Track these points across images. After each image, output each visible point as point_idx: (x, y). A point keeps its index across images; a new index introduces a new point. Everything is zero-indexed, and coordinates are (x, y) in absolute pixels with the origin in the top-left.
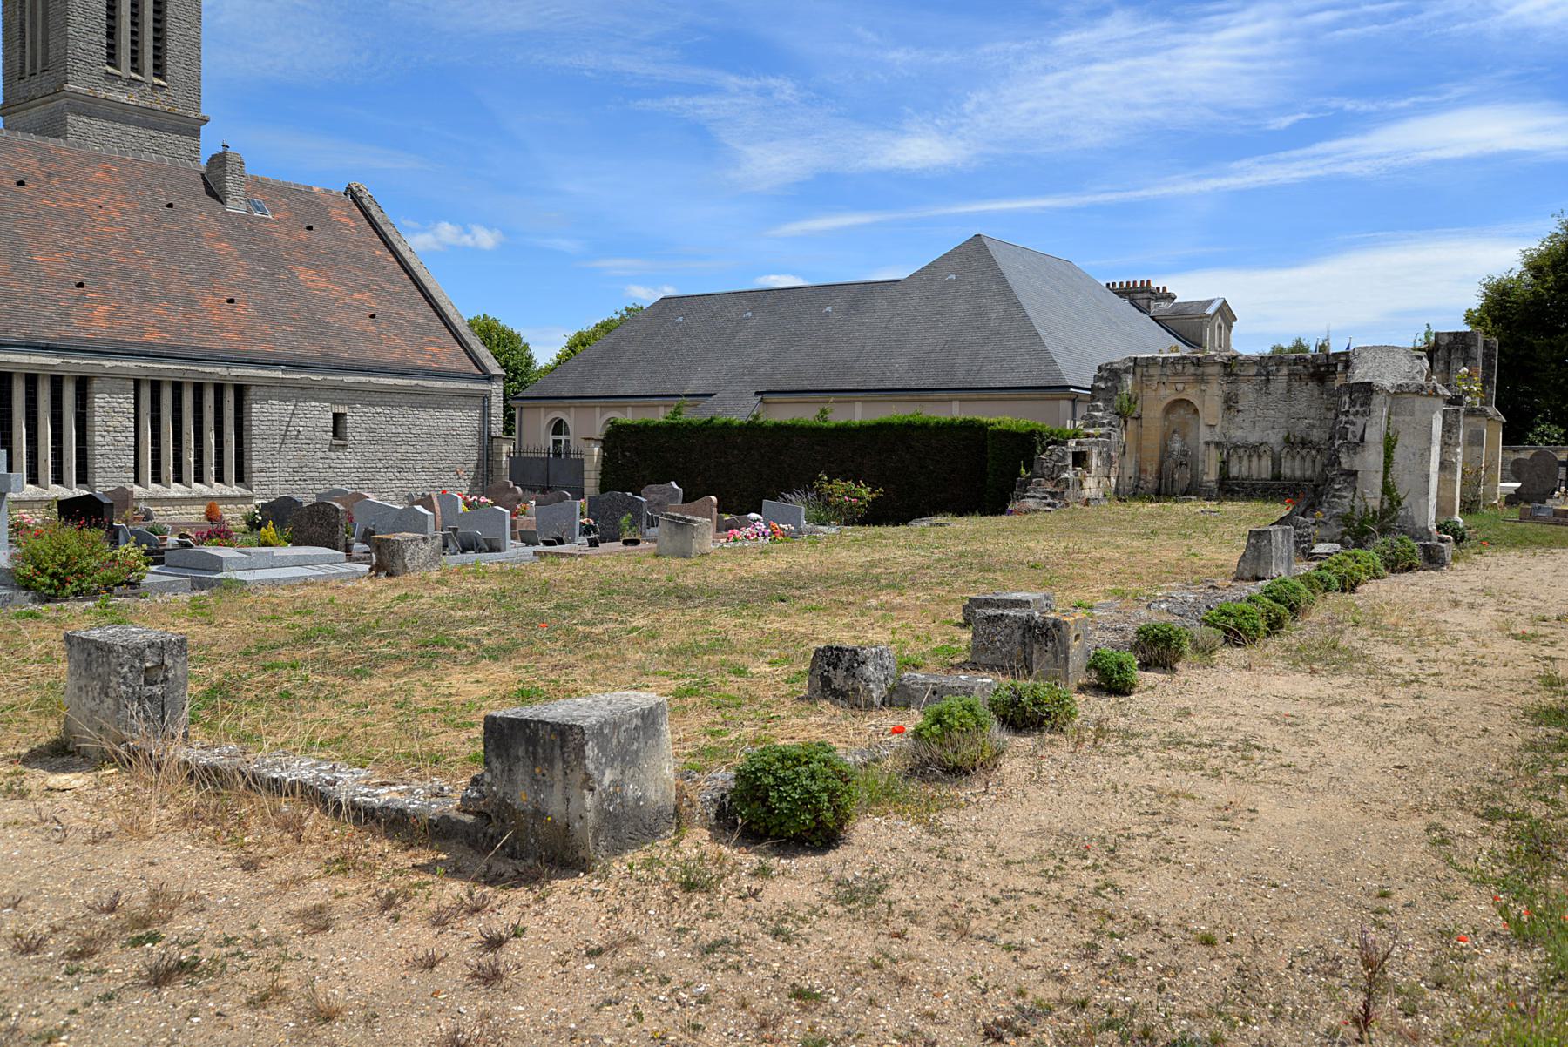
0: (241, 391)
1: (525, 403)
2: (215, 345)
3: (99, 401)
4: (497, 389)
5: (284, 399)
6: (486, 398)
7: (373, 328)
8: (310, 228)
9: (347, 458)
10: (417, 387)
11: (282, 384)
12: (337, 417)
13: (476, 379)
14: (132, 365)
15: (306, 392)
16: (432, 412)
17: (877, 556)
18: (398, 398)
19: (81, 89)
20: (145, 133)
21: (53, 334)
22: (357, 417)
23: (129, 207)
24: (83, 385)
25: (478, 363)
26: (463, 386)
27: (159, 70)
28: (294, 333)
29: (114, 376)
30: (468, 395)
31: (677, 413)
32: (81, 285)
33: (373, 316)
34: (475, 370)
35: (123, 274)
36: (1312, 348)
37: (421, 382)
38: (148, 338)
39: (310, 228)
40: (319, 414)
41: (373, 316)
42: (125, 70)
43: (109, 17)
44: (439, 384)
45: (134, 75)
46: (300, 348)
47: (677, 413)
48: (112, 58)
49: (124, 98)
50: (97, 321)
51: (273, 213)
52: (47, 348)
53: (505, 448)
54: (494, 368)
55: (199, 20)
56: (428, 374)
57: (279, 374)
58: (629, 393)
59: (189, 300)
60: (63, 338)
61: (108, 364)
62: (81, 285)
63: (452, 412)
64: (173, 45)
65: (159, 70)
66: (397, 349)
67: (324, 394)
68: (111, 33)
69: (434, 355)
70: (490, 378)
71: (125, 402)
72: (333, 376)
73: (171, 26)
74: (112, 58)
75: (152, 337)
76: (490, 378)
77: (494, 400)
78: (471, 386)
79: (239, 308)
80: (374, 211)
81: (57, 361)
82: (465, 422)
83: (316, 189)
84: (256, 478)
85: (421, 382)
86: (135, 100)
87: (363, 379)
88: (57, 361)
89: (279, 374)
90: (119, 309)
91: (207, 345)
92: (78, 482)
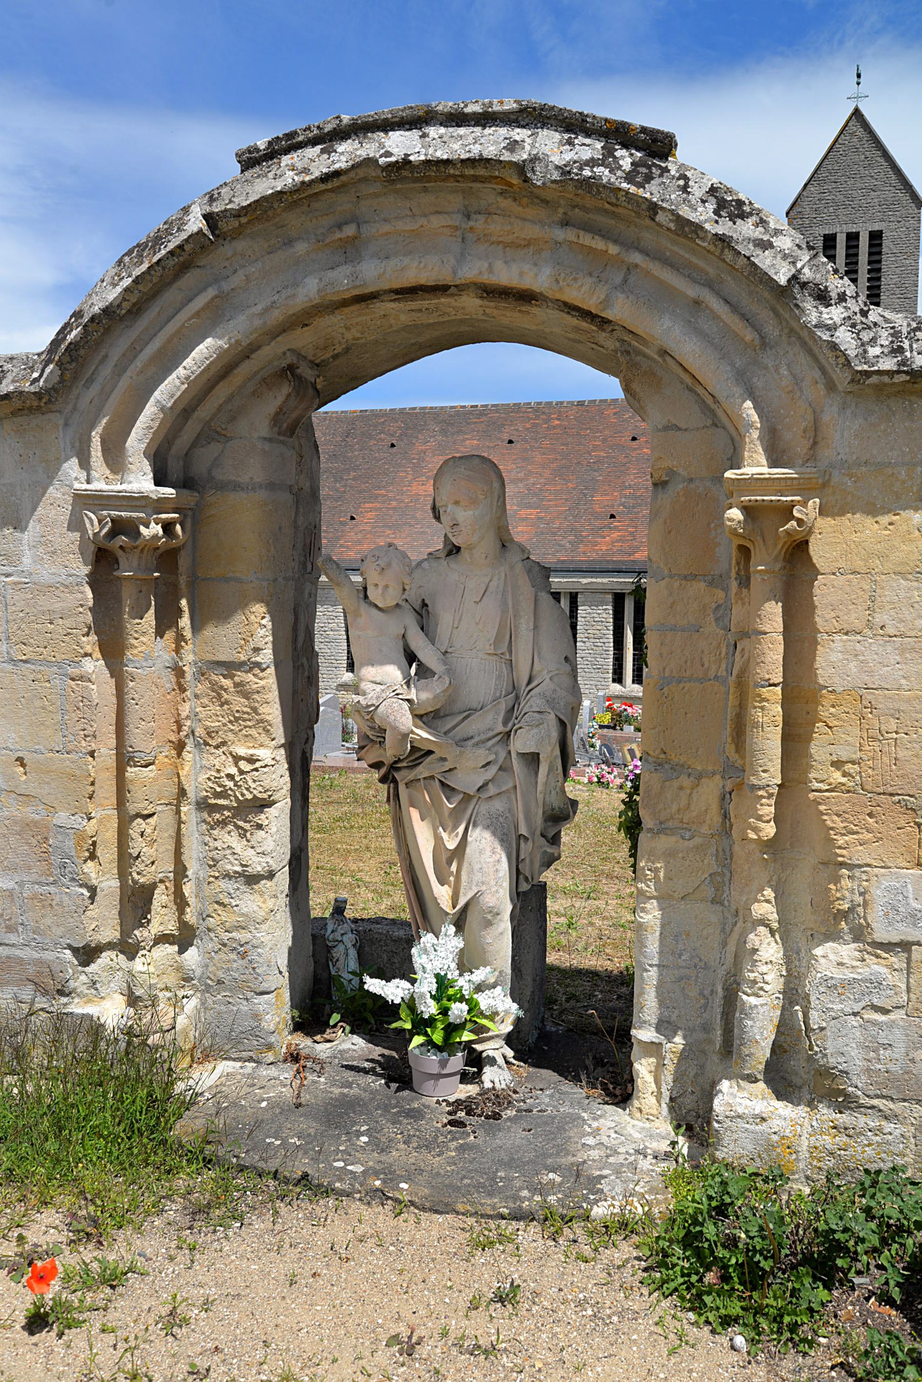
14: (605, 580)
61: (584, 581)
62: (612, 516)
71: (606, 614)
90: (631, 533)
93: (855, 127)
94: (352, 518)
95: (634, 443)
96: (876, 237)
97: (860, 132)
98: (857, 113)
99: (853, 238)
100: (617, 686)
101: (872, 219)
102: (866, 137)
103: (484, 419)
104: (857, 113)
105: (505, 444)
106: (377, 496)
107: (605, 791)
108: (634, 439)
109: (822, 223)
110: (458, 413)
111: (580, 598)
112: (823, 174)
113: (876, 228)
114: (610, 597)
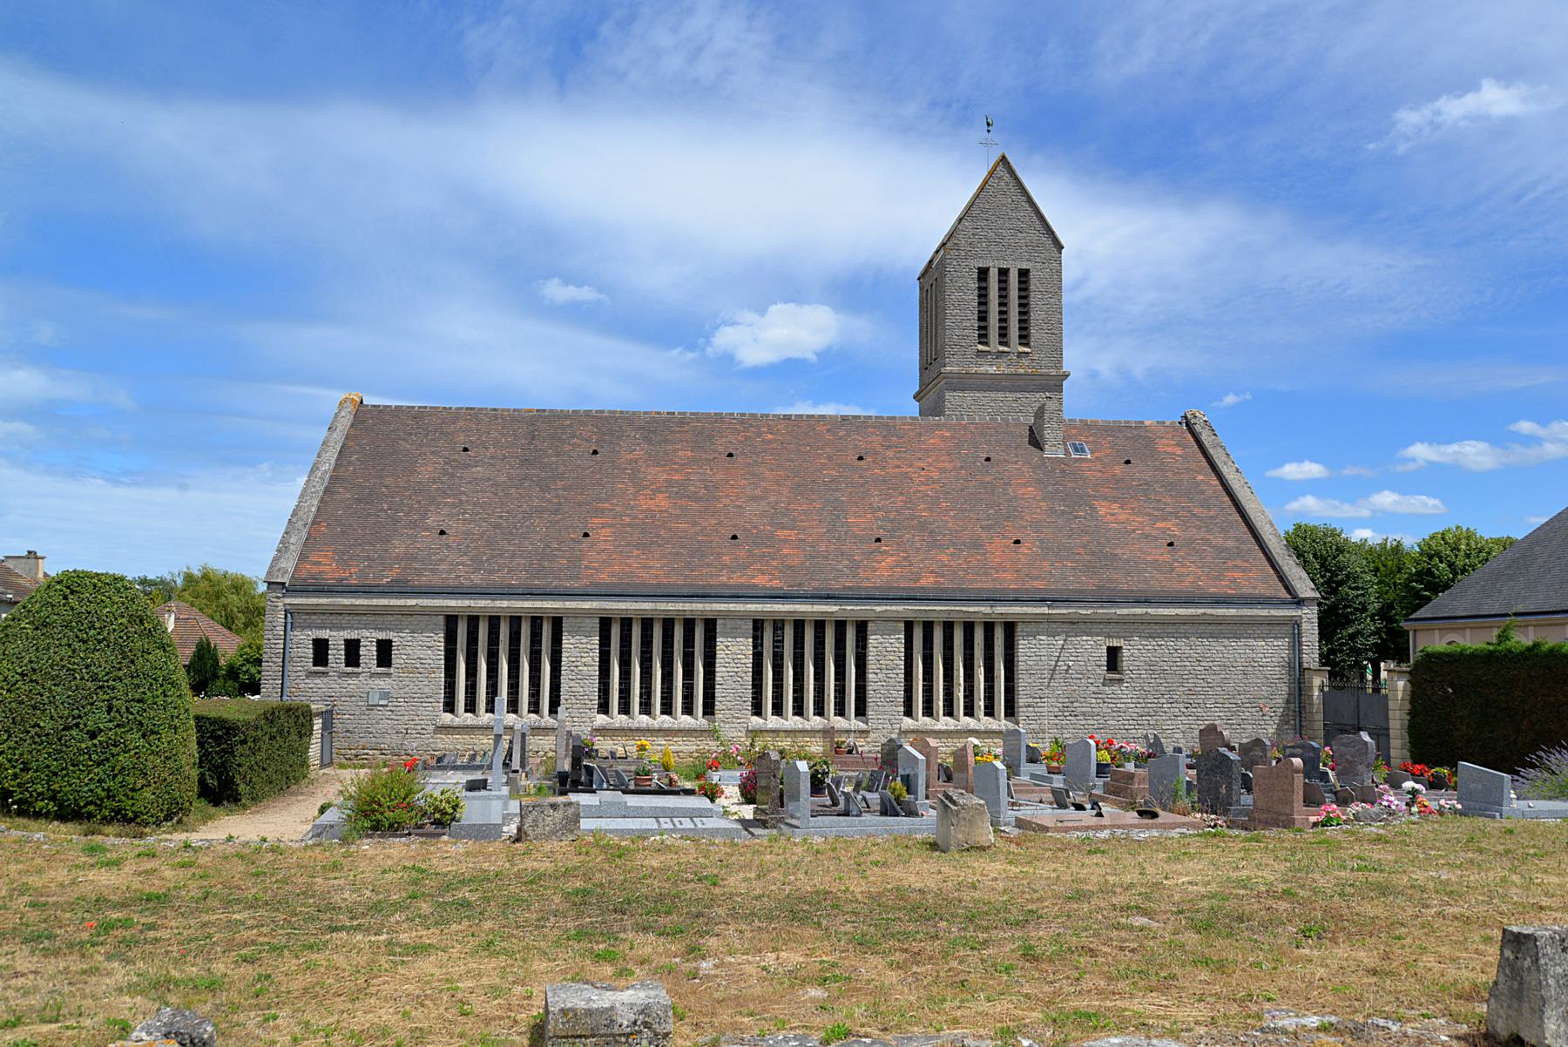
0: (1010, 628)
1: (1417, 625)
2: (985, 586)
3: (873, 641)
4: (1309, 618)
5: (1053, 635)
6: (1296, 624)
7: (1167, 557)
8: (1128, 462)
9: (1124, 694)
10: (1213, 616)
11: (1049, 619)
12: (1113, 654)
13: (1283, 603)
14: (900, 608)
15: (1075, 626)
16: (1226, 642)
17: (1123, 920)
18: (1182, 629)
19: (956, 369)
20: (1011, 396)
21: (836, 586)
22: (1133, 651)
23: (949, 466)
24: (862, 628)
25: (1288, 588)
26: (1264, 612)
27: (1024, 338)
28: (1073, 568)
29: (886, 619)
30: (1271, 623)
31: (1503, 637)
32: (878, 540)
33: (1171, 544)
34: (1284, 594)
35: (923, 526)
36: (179, 581)
37: (1209, 611)
38: (924, 582)
39: (1128, 462)
40: (1093, 649)
41: (1171, 544)
42: (994, 345)
43: (980, 296)
44: (1232, 612)
45: (1001, 348)
46: (1075, 582)
47: (1503, 637)
48: (983, 337)
49: (993, 370)
50: (884, 570)
51: (1092, 452)
52: (829, 597)
53: (1317, 681)
54: (1305, 586)
55: (1060, 288)
56: (1219, 601)
57: (1045, 610)
58: (1531, 609)
59: (976, 544)
60: (845, 588)
61: (878, 609)
62: (878, 540)
63: (1252, 642)
64: (1036, 316)
65: (1024, 338)
66: (1191, 575)
67: (1097, 628)
68: (983, 317)
69: (1234, 581)
70: (1299, 602)
71: (897, 642)
72: (1116, 613)
73: (1034, 299)
74: (983, 337)
75: (927, 581)
76: (1299, 602)
77: (1304, 626)
78: (1274, 612)
79: (1023, 549)
80: (1206, 437)
81: (835, 608)
82: (1271, 652)
83: (1147, 423)
84: (1022, 712)
85: (1209, 611)
86: (1004, 369)
87: (1139, 611)
88: (835, 608)
89: (1045, 610)
90: (905, 559)
91: (979, 585)
92: (857, 715)
93: (1001, 171)
94: (586, 535)
95: (861, 463)
96: (1024, 274)
97: (1007, 177)
98: (1003, 159)
99: (1003, 273)
100: (907, 720)
101: (1020, 258)
102: (1012, 183)
103: (686, 428)
104: (1003, 159)
105: (724, 457)
106: (603, 510)
107: (1288, 835)
108: (861, 458)
109: (976, 257)
110: (654, 420)
111: (871, 627)
112: (975, 211)
113: (1024, 266)
114: (441, 620)
